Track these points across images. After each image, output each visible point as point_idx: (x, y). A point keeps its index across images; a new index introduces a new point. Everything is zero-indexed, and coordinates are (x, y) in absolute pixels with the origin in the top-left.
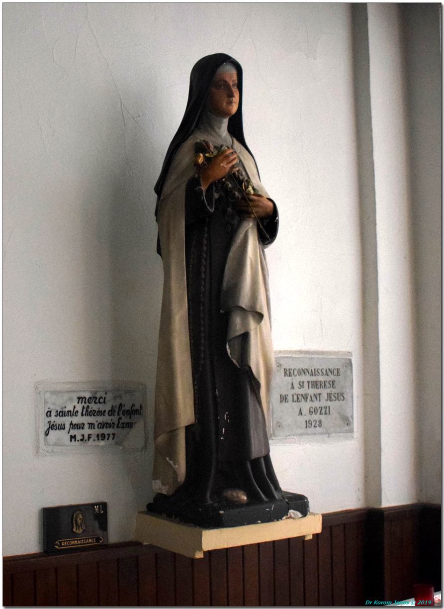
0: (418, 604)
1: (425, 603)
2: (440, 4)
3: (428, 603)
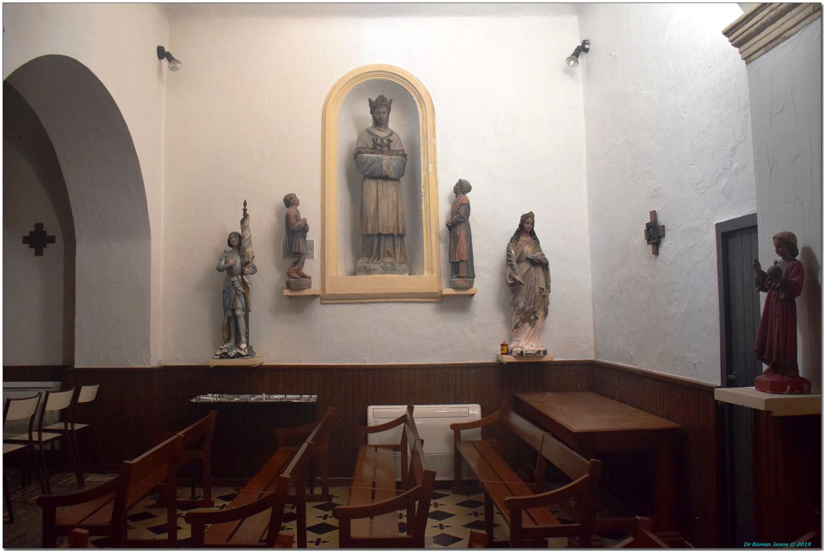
0: (798, 546)
1: (805, 544)
3: (807, 545)
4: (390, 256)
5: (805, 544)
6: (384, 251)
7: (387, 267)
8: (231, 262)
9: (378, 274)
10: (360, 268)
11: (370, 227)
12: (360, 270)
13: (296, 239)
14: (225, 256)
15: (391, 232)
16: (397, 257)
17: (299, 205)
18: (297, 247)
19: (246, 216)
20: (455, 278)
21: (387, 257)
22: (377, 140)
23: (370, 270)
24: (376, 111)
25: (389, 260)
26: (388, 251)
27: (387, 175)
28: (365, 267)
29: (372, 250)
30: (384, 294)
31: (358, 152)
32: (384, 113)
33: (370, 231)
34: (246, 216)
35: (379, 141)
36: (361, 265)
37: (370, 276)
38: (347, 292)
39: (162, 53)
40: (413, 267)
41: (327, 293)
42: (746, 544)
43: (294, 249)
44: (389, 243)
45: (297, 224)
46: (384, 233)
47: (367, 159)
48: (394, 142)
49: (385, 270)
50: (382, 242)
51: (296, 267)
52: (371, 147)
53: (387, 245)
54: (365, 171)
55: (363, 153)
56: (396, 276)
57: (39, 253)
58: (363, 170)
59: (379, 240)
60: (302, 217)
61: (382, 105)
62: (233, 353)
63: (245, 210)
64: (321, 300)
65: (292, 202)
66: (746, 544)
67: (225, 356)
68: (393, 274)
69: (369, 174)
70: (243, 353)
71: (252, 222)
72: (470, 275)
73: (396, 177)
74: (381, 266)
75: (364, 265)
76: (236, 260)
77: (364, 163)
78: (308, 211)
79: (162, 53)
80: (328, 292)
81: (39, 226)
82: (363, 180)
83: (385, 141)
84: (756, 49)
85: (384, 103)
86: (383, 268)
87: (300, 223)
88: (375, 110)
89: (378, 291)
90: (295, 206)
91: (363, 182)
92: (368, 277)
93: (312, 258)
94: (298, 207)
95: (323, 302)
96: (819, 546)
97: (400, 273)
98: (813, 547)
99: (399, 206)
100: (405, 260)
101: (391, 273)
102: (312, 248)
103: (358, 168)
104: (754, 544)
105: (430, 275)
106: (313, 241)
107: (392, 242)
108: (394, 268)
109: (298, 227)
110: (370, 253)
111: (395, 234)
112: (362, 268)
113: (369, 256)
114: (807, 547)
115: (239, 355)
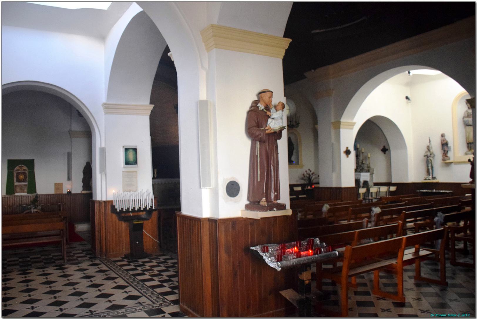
0: (462, 316)
1: (466, 315)
2: (475, 2)
5: (466, 315)
8: (427, 154)
14: (426, 152)
19: (430, 141)
34: (430, 141)
39: (407, 98)
42: (432, 315)
43: (269, 200)
57: (385, 153)
59: (471, 145)
62: (428, 179)
63: (429, 140)
66: (432, 315)
67: (425, 179)
70: (430, 179)
71: (432, 142)
76: (429, 154)
78: (449, 139)
79: (407, 98)
81: (384, 147)
84: (103, 185)
96: (474, 316)
98: (470, 317)
102: (451, 148)
104: (436, 315)
114: (468, 317)
115: (429, 179)
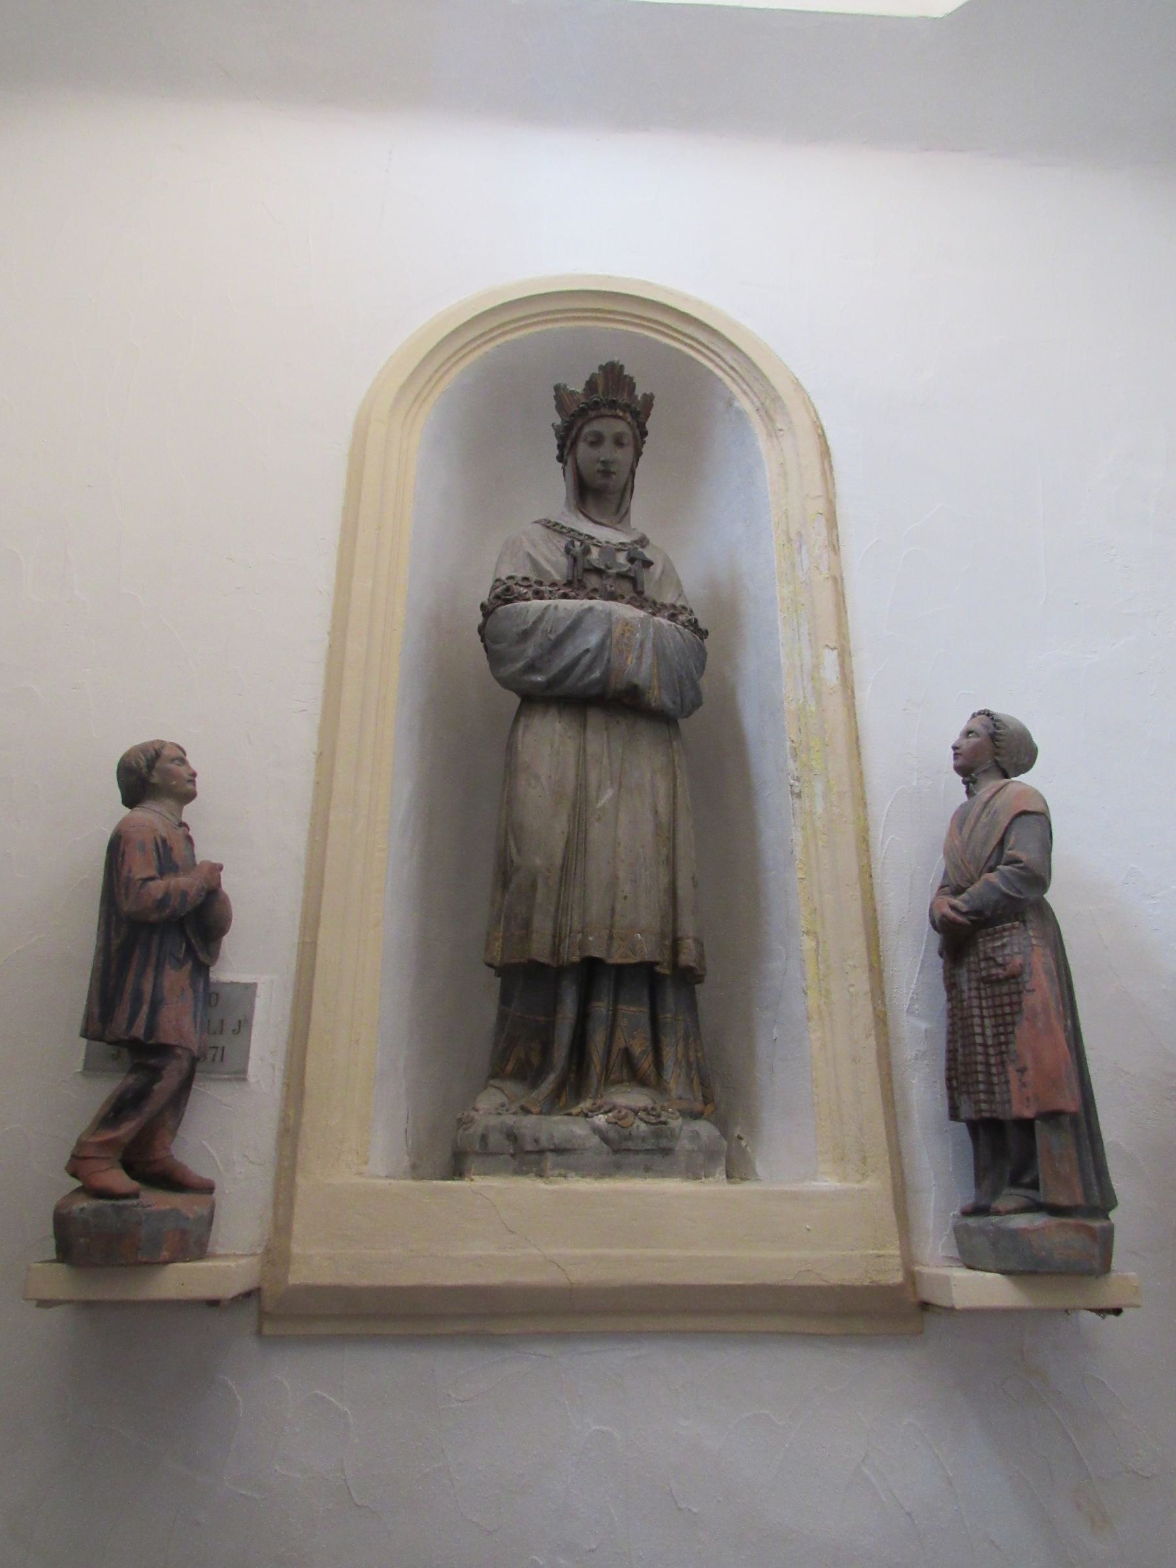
4: (637, 1079)
6: (608, 1051)
7: (630, 1137)
9: (584, 1171)
10: (484, 1138)
11: (543, 926)
12: (485, 1150)
13: (141, 974)
15: (647, 958)
16: (672, 1085)
17: (190, 796)
18: (145, 1008)
20: (1016, 1211)
21: (621, 1082)
22: (587, 551)
23: (541, 1152)
24: (587, 430)
25: (632, 1098)
26: (627, 1053)
27: (636, 687)
28: (512, 1136)
29: (546, 1049)
30: (638, 1335)
31: (497, 597)
32: (618, 442)
33: (540, 949)
35: (595, 553)
36: (494, 1121)
37: (540, 1184)
38: (407, 1278)
40: (738, 1131)
41: (294, 1280)
44: (634, 1013)
45: (158, 888)
46: (616, 959)
47: (540, 619)
48: (657, 570)
49: (616, 1152)
50: (601, 1007)
51: (126, 1130)
52: (557, 577)
53: (623, 1022)
54: (531, 668)
55: (523, 598)
56: (672, 1185)
58: (520, 664)
60: (205, 852)
61: (613, 404)
64: (263, 1315)
65: (155, 778)
68: (663, 1175)
69: (551, 684)
72: (1097, 1201)
73: (670, 705)
74: (596, 1130)
75: (509, 1119)
77: (526, 635)
80: (299, 1276)
82: (516, 720)
83: (622, 558)
85: (623, 399)
86: (605, 1139)
87: (181, 881)
88: (581, 429)
89: (579, 1276)
90: (171, 803)
91: (513, 730)
92: (528, 1187)
93: (240, 1075)
94: (188, 808)
95: (268, 1329)
97: (692, 1173)
99: (680, 836)
100: (707, 1100)
101: (648, 1170)
102: (244, 1025)
103: (495, 659)
105: (466, 1114)
106: (255, 985)
107: (646, 1009)
108: (664, 1143)
109: (162, 903)
110: (535, 1059)
111: (664, 970)
112: (495, 1139)
113: (529, 1075)
